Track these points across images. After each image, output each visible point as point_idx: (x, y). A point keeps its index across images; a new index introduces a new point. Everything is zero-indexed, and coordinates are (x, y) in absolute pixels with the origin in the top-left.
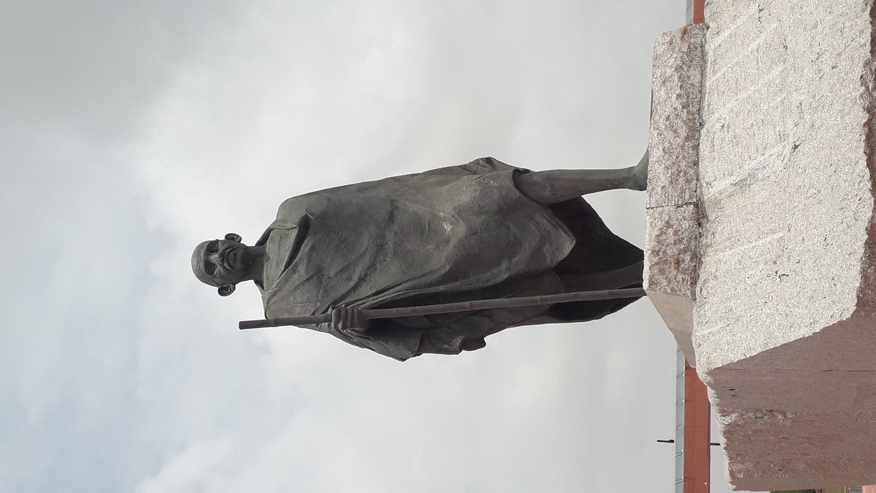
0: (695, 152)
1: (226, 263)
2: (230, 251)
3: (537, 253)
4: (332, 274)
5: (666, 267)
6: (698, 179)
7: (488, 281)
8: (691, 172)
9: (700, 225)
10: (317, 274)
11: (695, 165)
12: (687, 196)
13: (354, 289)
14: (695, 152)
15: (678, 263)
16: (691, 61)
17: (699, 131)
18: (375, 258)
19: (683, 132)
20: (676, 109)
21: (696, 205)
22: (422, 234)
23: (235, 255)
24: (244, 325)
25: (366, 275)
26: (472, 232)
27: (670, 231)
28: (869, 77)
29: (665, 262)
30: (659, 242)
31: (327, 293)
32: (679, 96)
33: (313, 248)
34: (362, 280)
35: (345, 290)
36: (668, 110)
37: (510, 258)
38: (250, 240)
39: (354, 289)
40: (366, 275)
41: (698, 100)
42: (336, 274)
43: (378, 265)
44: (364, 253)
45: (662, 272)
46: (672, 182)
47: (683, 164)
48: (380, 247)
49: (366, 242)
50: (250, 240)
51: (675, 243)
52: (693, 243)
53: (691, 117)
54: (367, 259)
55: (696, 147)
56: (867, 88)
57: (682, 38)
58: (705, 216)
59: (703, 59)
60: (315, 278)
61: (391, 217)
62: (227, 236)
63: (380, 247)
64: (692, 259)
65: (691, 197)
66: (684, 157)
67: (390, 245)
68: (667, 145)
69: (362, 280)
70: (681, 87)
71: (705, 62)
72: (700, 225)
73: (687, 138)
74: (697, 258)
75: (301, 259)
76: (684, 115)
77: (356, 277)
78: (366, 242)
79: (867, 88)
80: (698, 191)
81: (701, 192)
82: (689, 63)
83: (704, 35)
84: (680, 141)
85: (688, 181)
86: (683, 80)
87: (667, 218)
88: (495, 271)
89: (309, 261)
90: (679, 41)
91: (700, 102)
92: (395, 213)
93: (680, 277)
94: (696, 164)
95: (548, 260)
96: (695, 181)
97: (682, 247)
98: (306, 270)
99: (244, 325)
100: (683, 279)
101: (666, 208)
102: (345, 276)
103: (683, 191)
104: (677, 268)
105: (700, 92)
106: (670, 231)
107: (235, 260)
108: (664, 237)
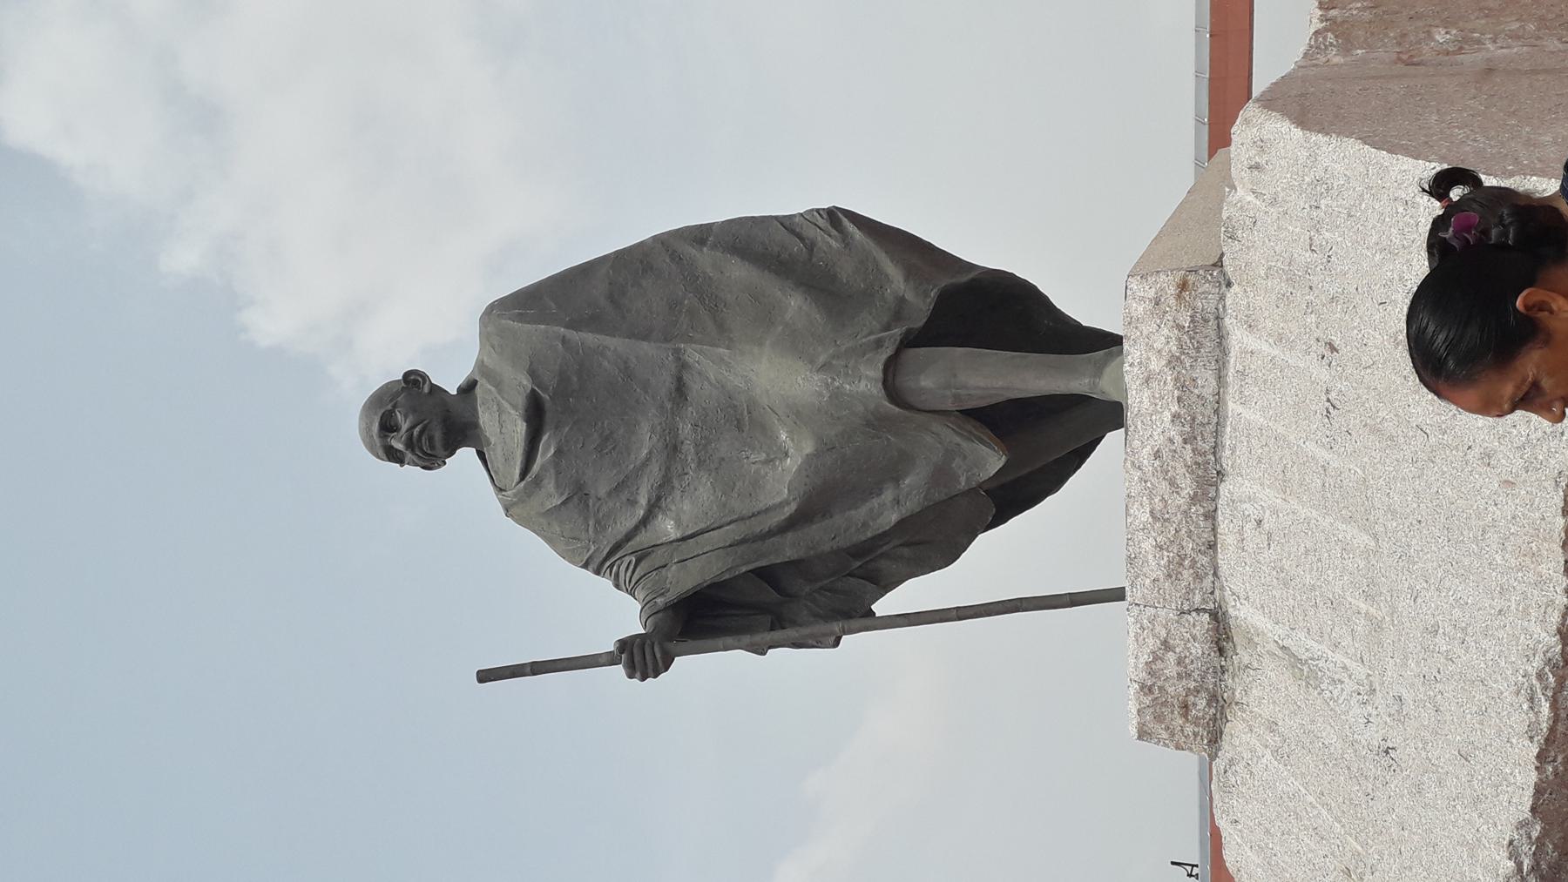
0: (1209, 524)
1: (419, 423)
2: (421, 433)
3: (941, 474)
4: (602, 492)
5: (1166, 710)
6: (1215, 574)
7: (865, 525)
8: (1204, 560)
9: (1221, 651)
10: (578, 495)
11: (1210, 547)
12: (1198, 598)
13: (644, 522)
14: (1209, 524)
15: (1185, 707)
16: (1198, 350)
17: (1216, 485)
18: (668, 469)
19: (1187, 486)
20: (1171, 441)
22: (739, 427)
23: (431, 439)
24: (485, 676)
25: (659, 498)
26: (825, 447)
27: (1171, 657)
28: (1525, 848)
29: (1165, 704)
30: (1152, 673)
31: (600, 526)
32: (1176, 416)
33: (559, 452)
34: (653, 508)
35: (626, 523)
36: (1159, 440)
37: (896, 480)
38: (450, 383)
39: (644, 522)
40: (659, 498)
41: (1211, 428)
42: (609, 494)
43: (676, 483)
44: (648, 459)
45: (1159, 718)
46: (1170, 576)
47: (1189, 546)
48: (673, 449)
49: (646, 441)
50: (450, 383)
51: (1180, 677)
52: (1210, 679)
53: (1200, 460)
54: (655, 470)
55: (1211, 516)
56: (1519, 865)
57: (1179, 297)
58: (1229, 638)
59: (1220, 344)
60: (576, 499)
61: (680, 390)
62: (407, 375)
63: (673, 449)
64: (1209, 704)
65: (1204, 601)
66: (1190, 534)
67: (688, 448)
68: (1159, 506)
69: (653, 508)
70: (1179, 400)
72: (1221, 651)
73: (1194, 499)
74: (1220, 704)
75: (543, 468)
76: (1188, 454)
77: (643, 501)
78: (646, 441)
79: (1519, 865)
80: (1217, 592)
81: (1223, 598)
82: (1193, 353)
83: (1222, 298)
84: (1181, 501)
85: (1198, 577)
86: (1184, 387)
87: (1163, 634)
88: (875, 502)
89: (558, 473)
90: (1172, 301)
91: (1217, 433)
92: (686, 377)
93: (1189, 729)
94: (1212, 546)
95: (963, 480)
96: (1211, 578)
97: (1192, 685)
98: (558, 486)
99: (485, 676)
100: (1195, 734)
101: (1162, 613)
102: (624, 496)
103: (1190, 591)
104: (1185, 716)
105: (1216, 412)
106: (1171, 657)
107: (432, 447)
108: (1159, 664)
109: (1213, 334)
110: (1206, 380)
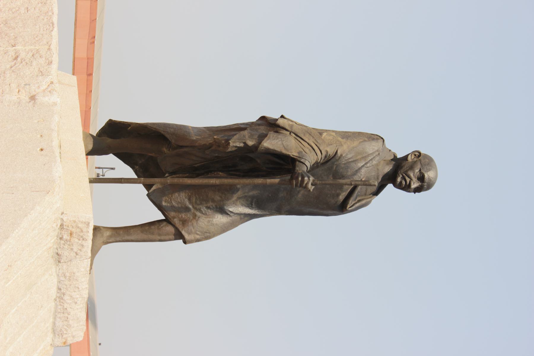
21: (59, 262)
110: (59, 323)
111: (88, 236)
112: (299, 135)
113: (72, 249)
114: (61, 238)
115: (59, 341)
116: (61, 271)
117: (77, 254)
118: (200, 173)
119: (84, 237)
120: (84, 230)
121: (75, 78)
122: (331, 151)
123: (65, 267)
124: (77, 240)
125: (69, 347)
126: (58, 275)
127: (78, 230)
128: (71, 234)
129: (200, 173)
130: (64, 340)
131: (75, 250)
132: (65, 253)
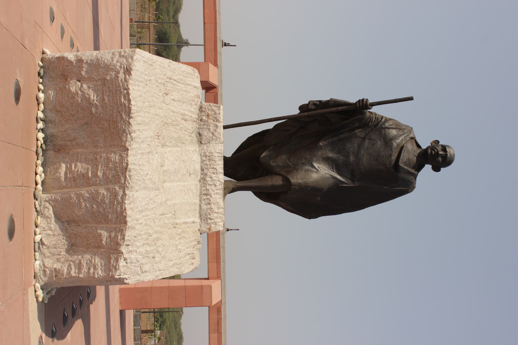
1: (437, 157)
21: (201, 143)
24: (411, 99)
71: (200, 213)
99: (411, 99)
109: (203, 217)
110: (204, 207)
111: (220, 118)
112: (214, 29)
113: (209, 129)
114: (201, 120)
115: (205, 228)
116: (203, 151)
117: (213, 134)
118: (11, 234)
119: (218, 118)
120: (217, 112)
121: (297, 112)
122: (132, 124)
123: (205, 147)
124: (212, 121)
125: (207, 277)
126: (201, 155)
127: (213, 113)
128: (208, 116)
129: (11, 234)
130: (209, 227)
131: (212, 130)
132: (205, 133)
